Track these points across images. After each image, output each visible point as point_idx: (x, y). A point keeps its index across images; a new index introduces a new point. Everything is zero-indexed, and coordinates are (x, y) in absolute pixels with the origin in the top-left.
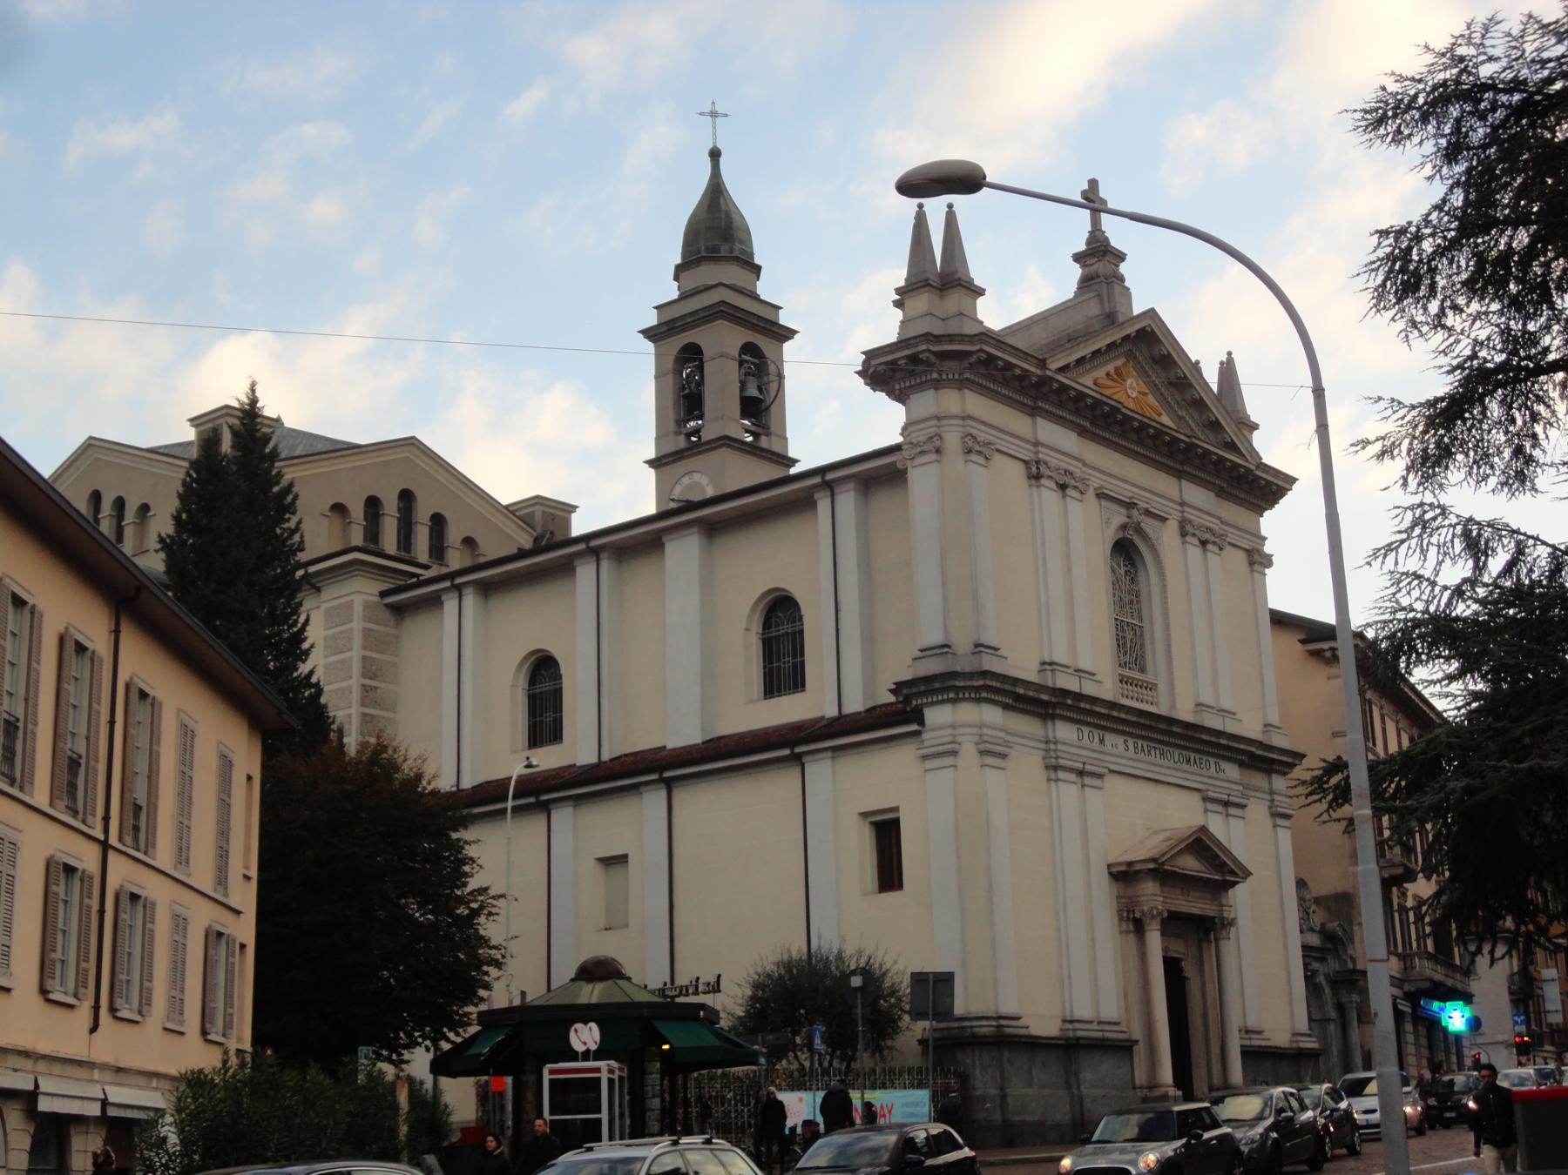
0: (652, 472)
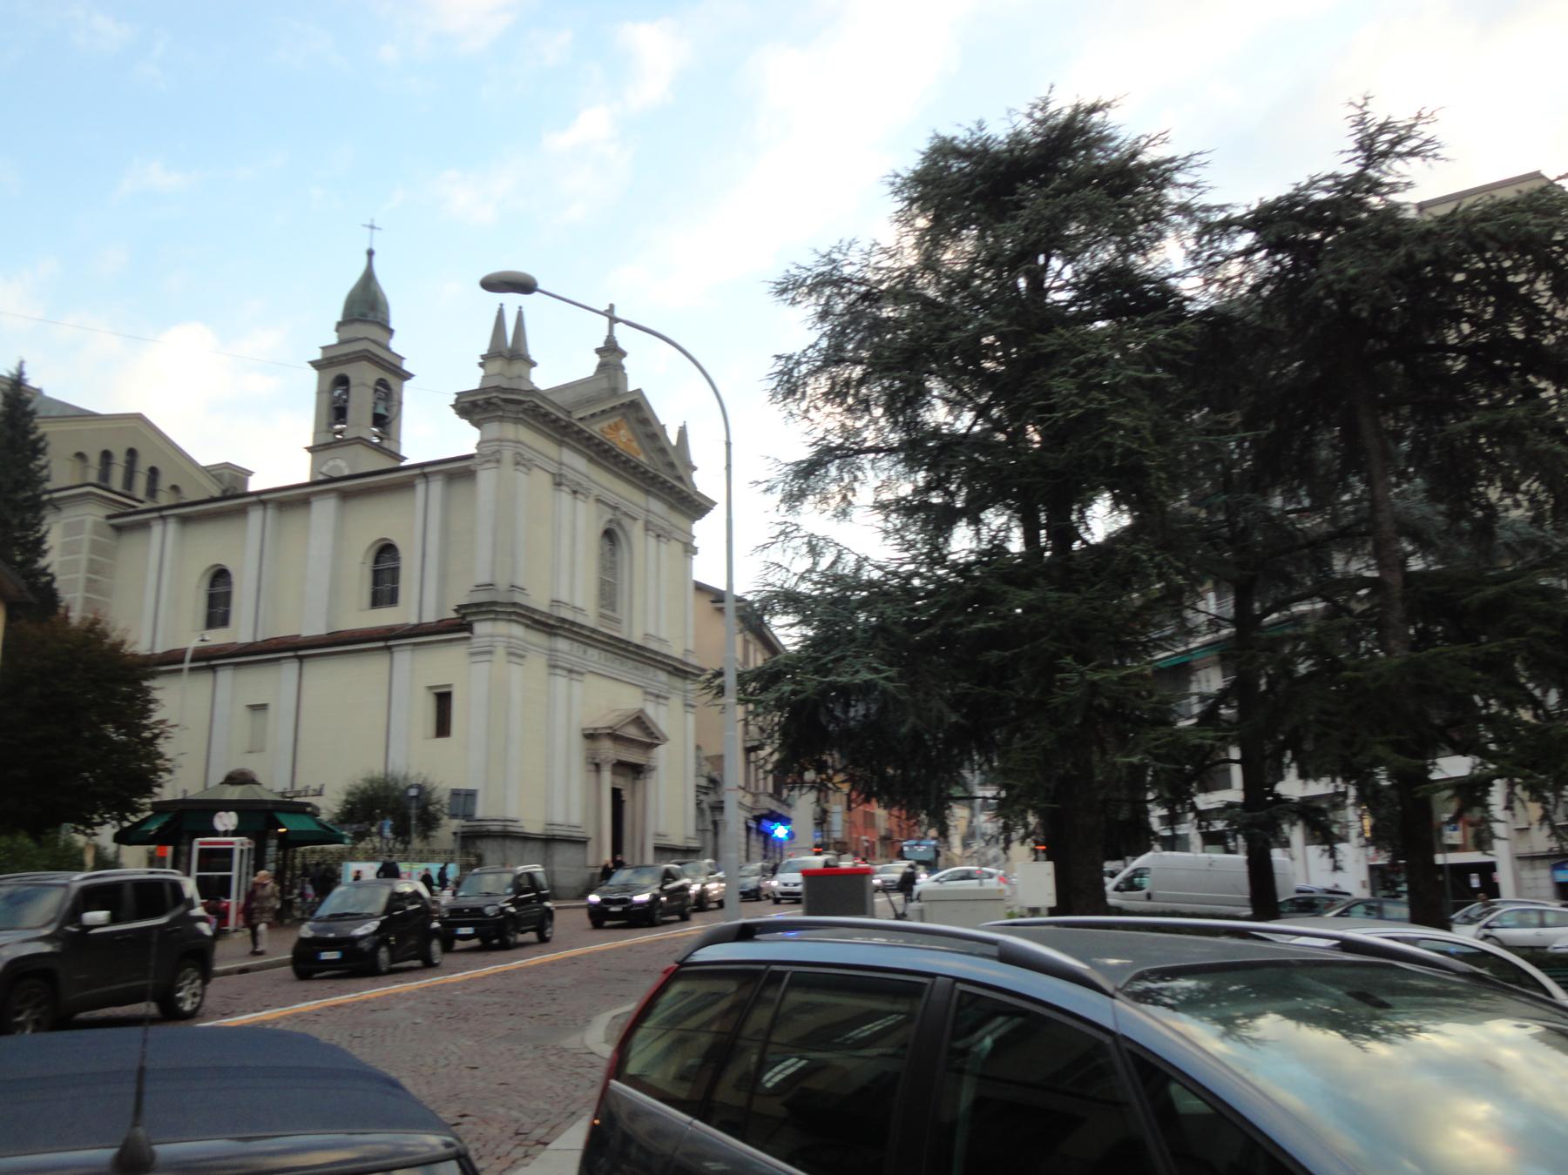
0: (309, 455)
